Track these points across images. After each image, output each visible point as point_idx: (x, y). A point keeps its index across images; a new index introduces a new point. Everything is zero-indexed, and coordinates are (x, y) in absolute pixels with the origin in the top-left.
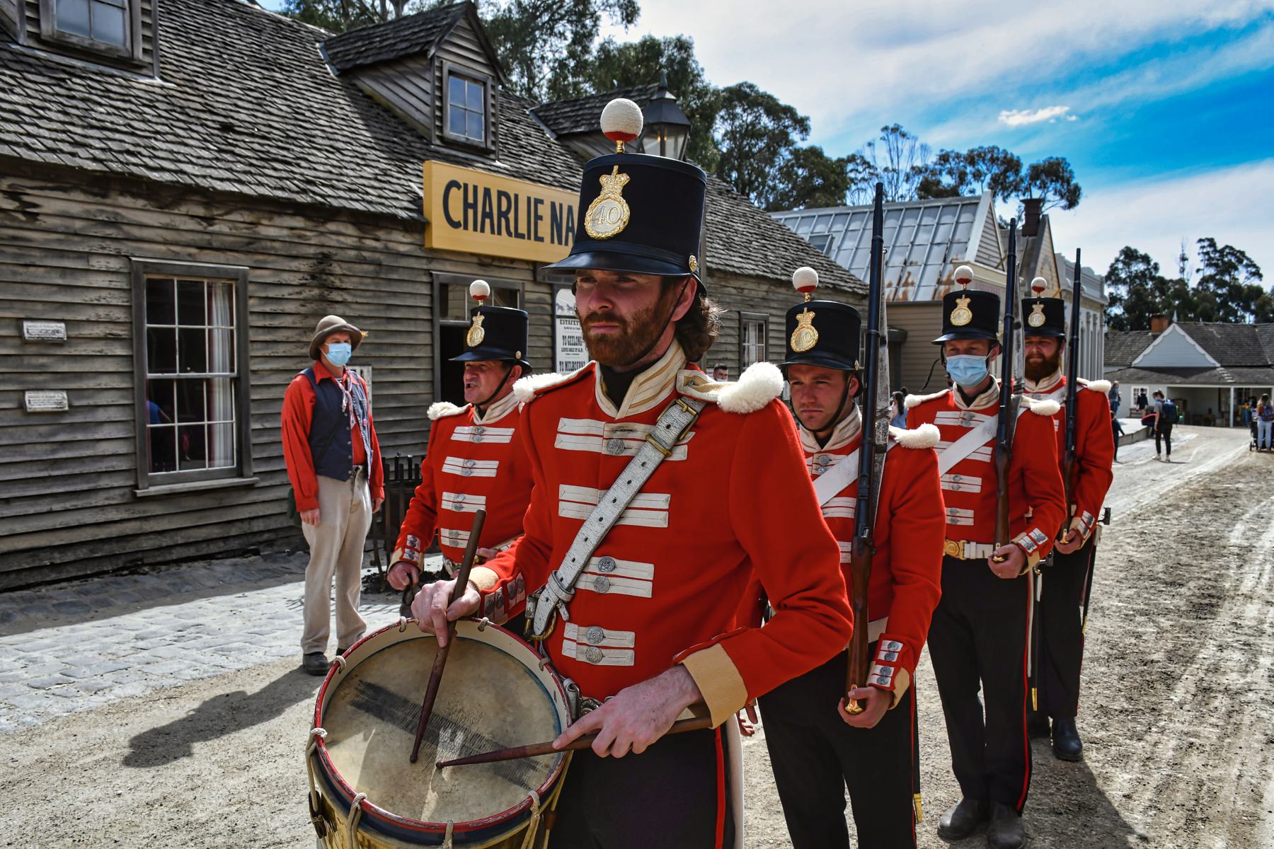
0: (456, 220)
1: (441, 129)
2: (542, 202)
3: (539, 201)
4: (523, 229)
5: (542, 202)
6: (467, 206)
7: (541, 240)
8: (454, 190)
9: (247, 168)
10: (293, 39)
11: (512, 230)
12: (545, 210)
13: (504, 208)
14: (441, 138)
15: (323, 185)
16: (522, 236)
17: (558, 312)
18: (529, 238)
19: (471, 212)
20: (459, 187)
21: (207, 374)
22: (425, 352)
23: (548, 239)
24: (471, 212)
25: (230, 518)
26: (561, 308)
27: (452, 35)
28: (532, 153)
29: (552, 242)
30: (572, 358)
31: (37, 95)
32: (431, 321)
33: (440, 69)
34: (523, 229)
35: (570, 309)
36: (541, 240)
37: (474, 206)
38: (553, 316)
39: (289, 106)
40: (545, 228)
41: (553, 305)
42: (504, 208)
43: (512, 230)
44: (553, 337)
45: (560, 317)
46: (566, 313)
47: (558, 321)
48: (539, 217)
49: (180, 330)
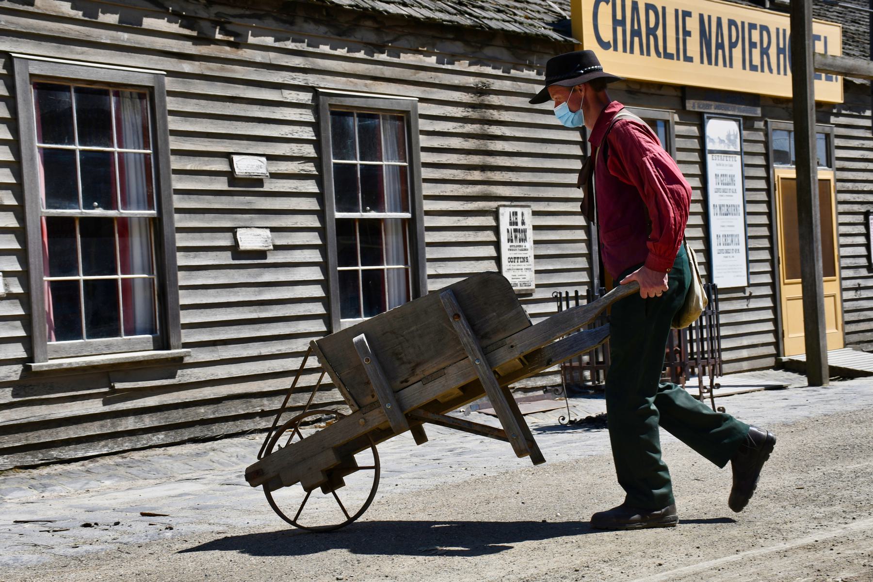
0: (605, 40)
11: (661, 49)
17: (709, 146)
22: (430, 270)
29: (702, 62)
34: (671, 48)
35: (722, 141)
37: (623, 23)
38: (702, 152)
40: (693, 45)
41: (702, 138)
43: (661, 49)
45: (712, 152)
47: (709, 157)
48: (687, 33)
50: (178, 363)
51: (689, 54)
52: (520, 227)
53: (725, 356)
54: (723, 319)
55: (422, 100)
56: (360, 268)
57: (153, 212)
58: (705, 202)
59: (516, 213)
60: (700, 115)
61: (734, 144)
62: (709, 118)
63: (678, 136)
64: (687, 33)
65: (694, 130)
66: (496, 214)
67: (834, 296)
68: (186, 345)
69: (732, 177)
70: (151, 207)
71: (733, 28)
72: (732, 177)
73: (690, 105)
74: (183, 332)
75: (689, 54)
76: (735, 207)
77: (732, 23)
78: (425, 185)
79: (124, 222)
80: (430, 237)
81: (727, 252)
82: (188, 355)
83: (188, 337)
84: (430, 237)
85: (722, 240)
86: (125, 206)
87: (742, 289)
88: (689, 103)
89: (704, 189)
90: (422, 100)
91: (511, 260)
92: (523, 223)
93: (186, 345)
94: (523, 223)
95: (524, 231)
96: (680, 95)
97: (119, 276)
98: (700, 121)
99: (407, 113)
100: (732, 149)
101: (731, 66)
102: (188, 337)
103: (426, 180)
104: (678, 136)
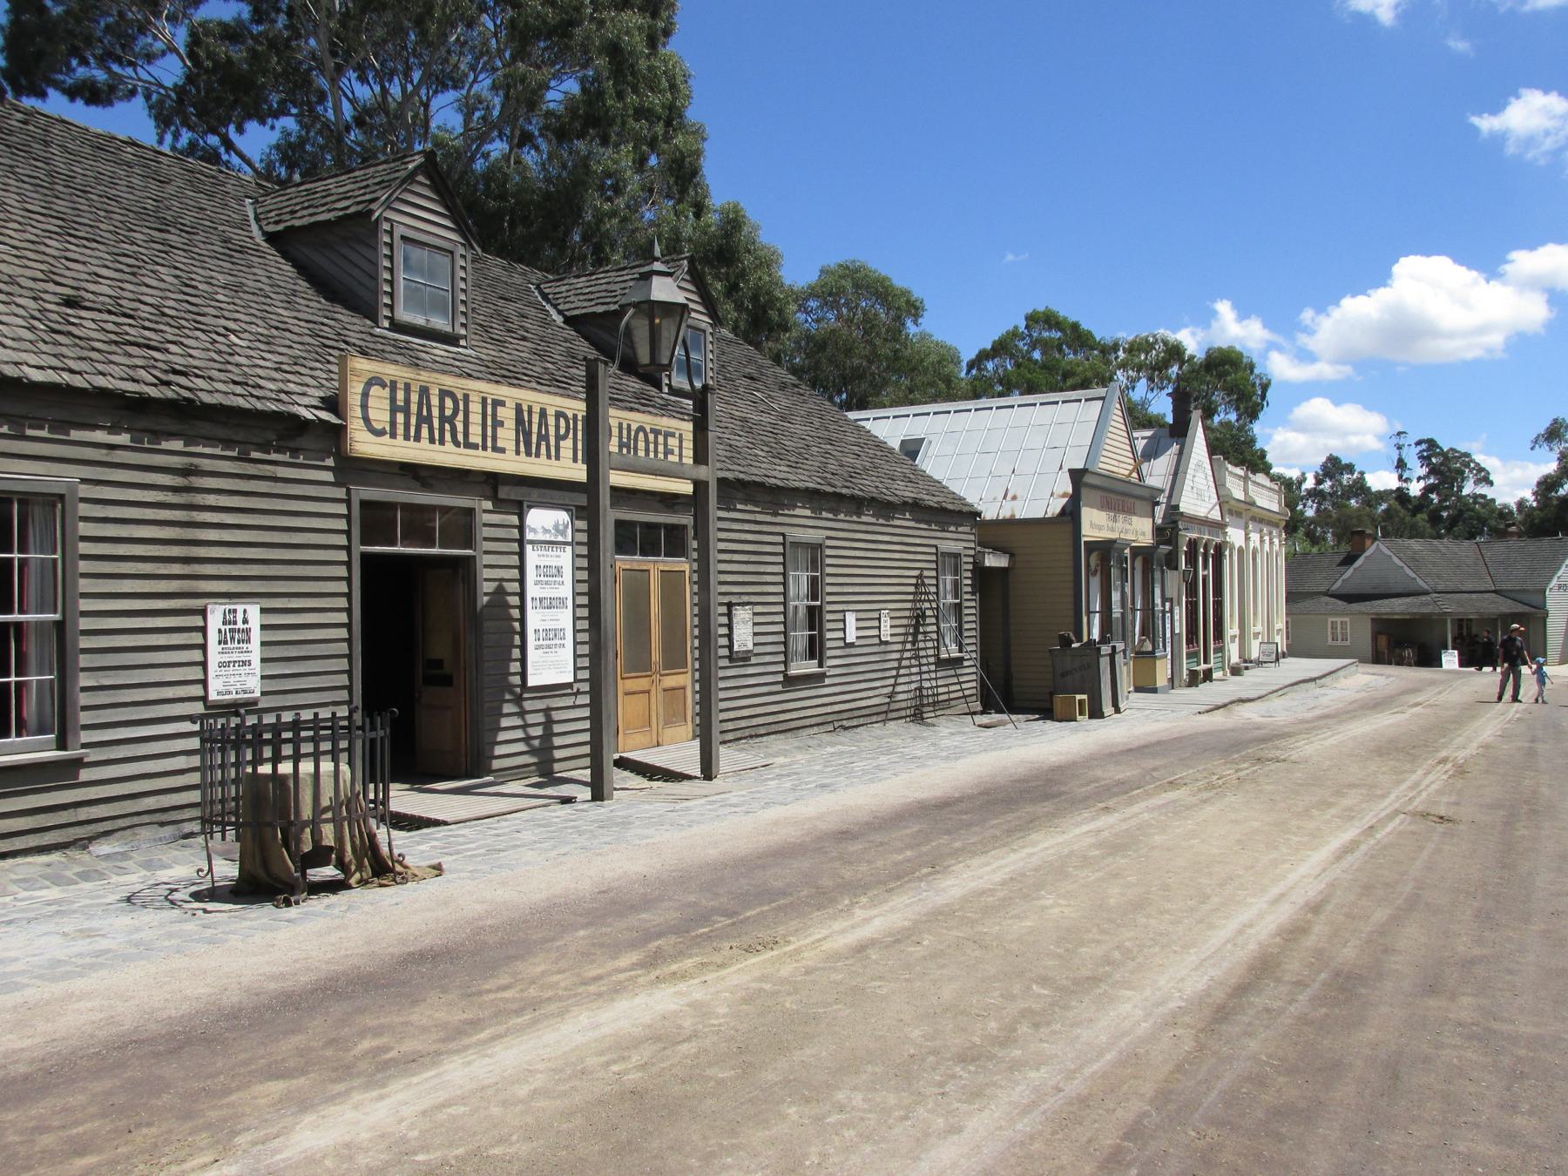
0: (378, 426)
1: (391, 307)
2: (503, 404)
3: (498, 403)
4: (475, 438)
5: (503, 404)
6: (394, 410)
7: (503, 451)
8: (375, 390)
9: (85, 353)
10: (211, 196)
11: (460, 438)
12: (507, 414)
13: (448, 412)
14: (391, 319)
15: (197, 376)
16: (475, 447)
17: (529, 536)
18: (485, 448)
19: (400, 418)
20: (384, 386)
21: (15, 617)
22: (85, 680)
23: (511, 446)
24: (400, 418)
25: (112, 757)
26: (534, 531)
27: (406, 190)
28: (524, 339)
29: (518, 452)
30: (548, 593)
31: (16, 261)
32: (348, 549)
33: (391, 233)
34: (475, 438)
35: (546, 531)
36: (503, 451)
37: (406, 410)
38: (521, 542)
39: (176, 277)
40: (507, 436)
41: (521, 528)
42: (448, 412)
43: (460, 438)
44: (522, 568)
45: (532, 542)
46: (541, 537)
47: (529, 548)
48: (497, 424)
49: (11, 552)
50: (78, 763)
51: (500, 444)
52: (240, 625)
53: (558, 754)
54: (195, 778)
55: (84, 481)
56: (13, 679)
57: (57, 617)
58: (522, 595)
59: (235, 611)
60: (520, 503)
61: (563, 533)
62: (530, 507)
63: (485, 525)
64: (497, 424)
65: (515, 520)
66: (203, 612)
67: (684, 688)
68: (84, 746)
69: (559, 569)
70: (55, 612)
71: (562, 421)
72: (559, 569)
73: (504, 492)
74: (83, 733)
75: (500, 444)
76: (562, 601)
77: (559, 415)
78: (82, 581)
79: (19, 626)
80: (85, 642)
81: (549, 647)
82: (87, 755)
83: (86, 736)
84: (85, 642)
85: (542, 635)
86: (21, 611)
87: (569, 685)
88: (514, 493)
89: (522, 581)
90: (84, 481)
91: (222, 665)
92: (245, 621)
93: (84, 746)
94: (245, 621)
95: (248, 631)
96: (491, 483)
97: (13, 679)
98: (520, 510)
99: (61, 497)
100: (560, 539)
101: (558, 458)
102: (86, 736)
103: (84, 575)
104: (485, 525)
